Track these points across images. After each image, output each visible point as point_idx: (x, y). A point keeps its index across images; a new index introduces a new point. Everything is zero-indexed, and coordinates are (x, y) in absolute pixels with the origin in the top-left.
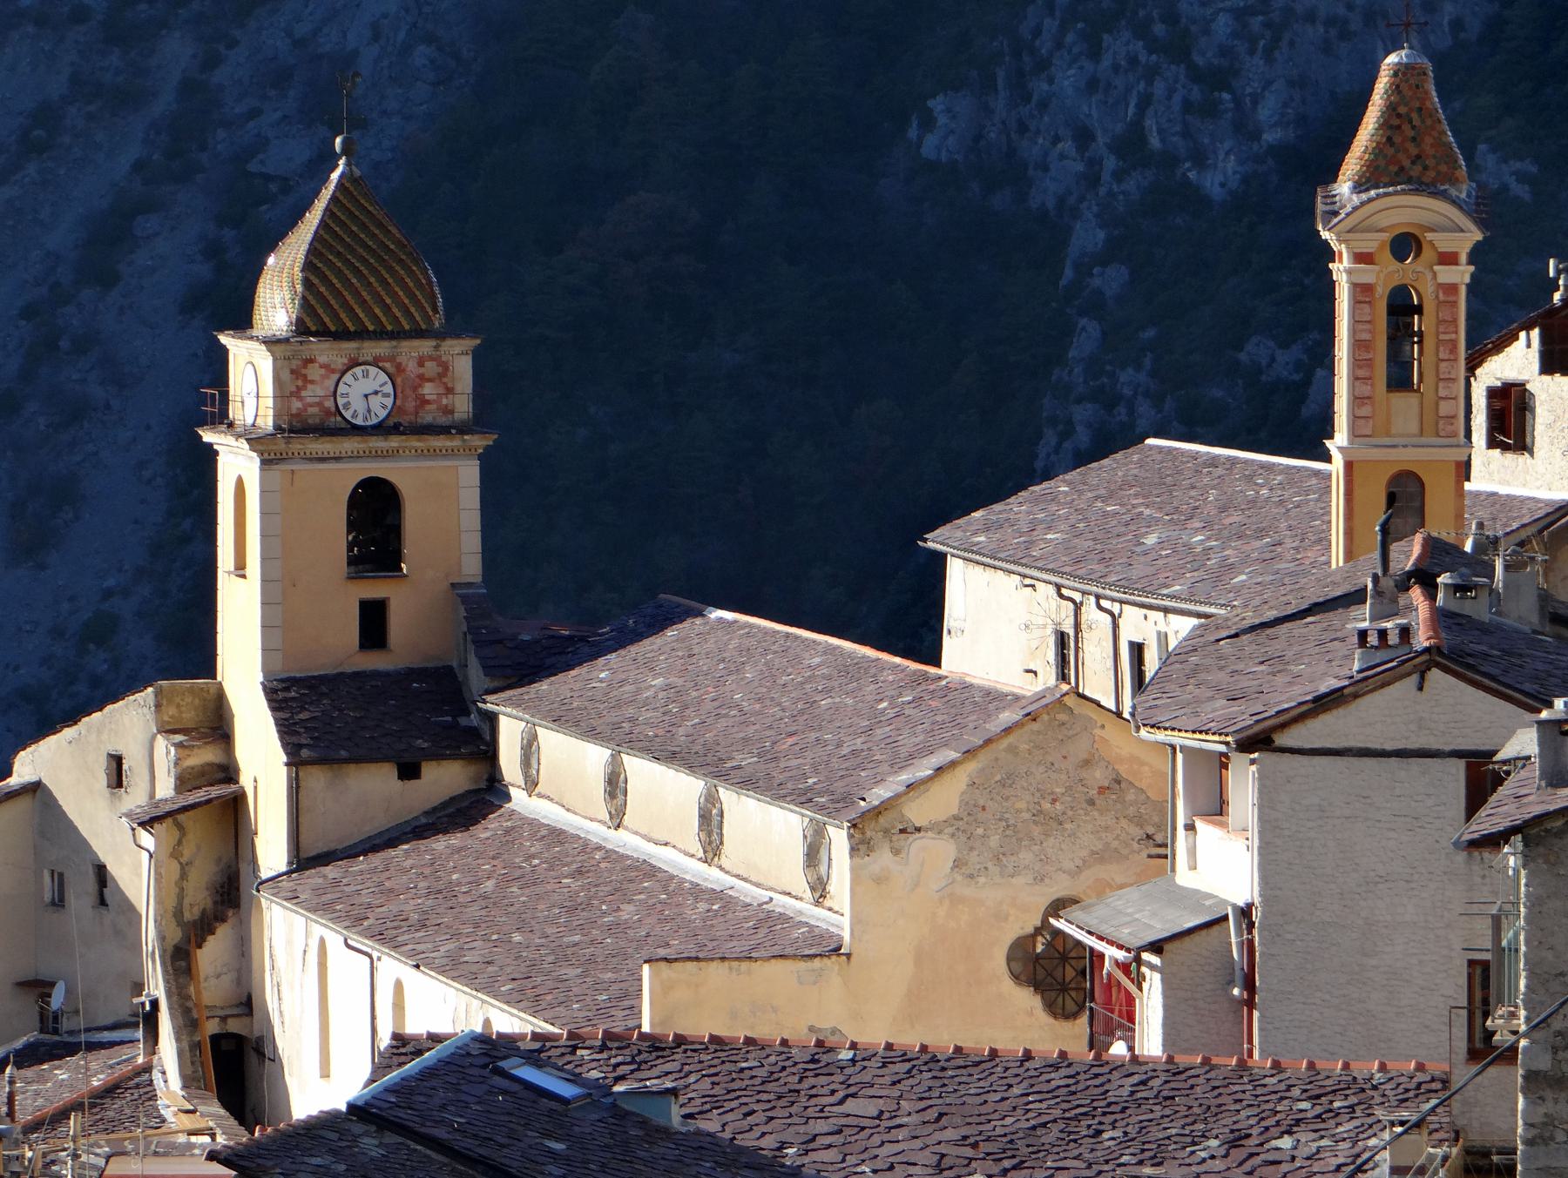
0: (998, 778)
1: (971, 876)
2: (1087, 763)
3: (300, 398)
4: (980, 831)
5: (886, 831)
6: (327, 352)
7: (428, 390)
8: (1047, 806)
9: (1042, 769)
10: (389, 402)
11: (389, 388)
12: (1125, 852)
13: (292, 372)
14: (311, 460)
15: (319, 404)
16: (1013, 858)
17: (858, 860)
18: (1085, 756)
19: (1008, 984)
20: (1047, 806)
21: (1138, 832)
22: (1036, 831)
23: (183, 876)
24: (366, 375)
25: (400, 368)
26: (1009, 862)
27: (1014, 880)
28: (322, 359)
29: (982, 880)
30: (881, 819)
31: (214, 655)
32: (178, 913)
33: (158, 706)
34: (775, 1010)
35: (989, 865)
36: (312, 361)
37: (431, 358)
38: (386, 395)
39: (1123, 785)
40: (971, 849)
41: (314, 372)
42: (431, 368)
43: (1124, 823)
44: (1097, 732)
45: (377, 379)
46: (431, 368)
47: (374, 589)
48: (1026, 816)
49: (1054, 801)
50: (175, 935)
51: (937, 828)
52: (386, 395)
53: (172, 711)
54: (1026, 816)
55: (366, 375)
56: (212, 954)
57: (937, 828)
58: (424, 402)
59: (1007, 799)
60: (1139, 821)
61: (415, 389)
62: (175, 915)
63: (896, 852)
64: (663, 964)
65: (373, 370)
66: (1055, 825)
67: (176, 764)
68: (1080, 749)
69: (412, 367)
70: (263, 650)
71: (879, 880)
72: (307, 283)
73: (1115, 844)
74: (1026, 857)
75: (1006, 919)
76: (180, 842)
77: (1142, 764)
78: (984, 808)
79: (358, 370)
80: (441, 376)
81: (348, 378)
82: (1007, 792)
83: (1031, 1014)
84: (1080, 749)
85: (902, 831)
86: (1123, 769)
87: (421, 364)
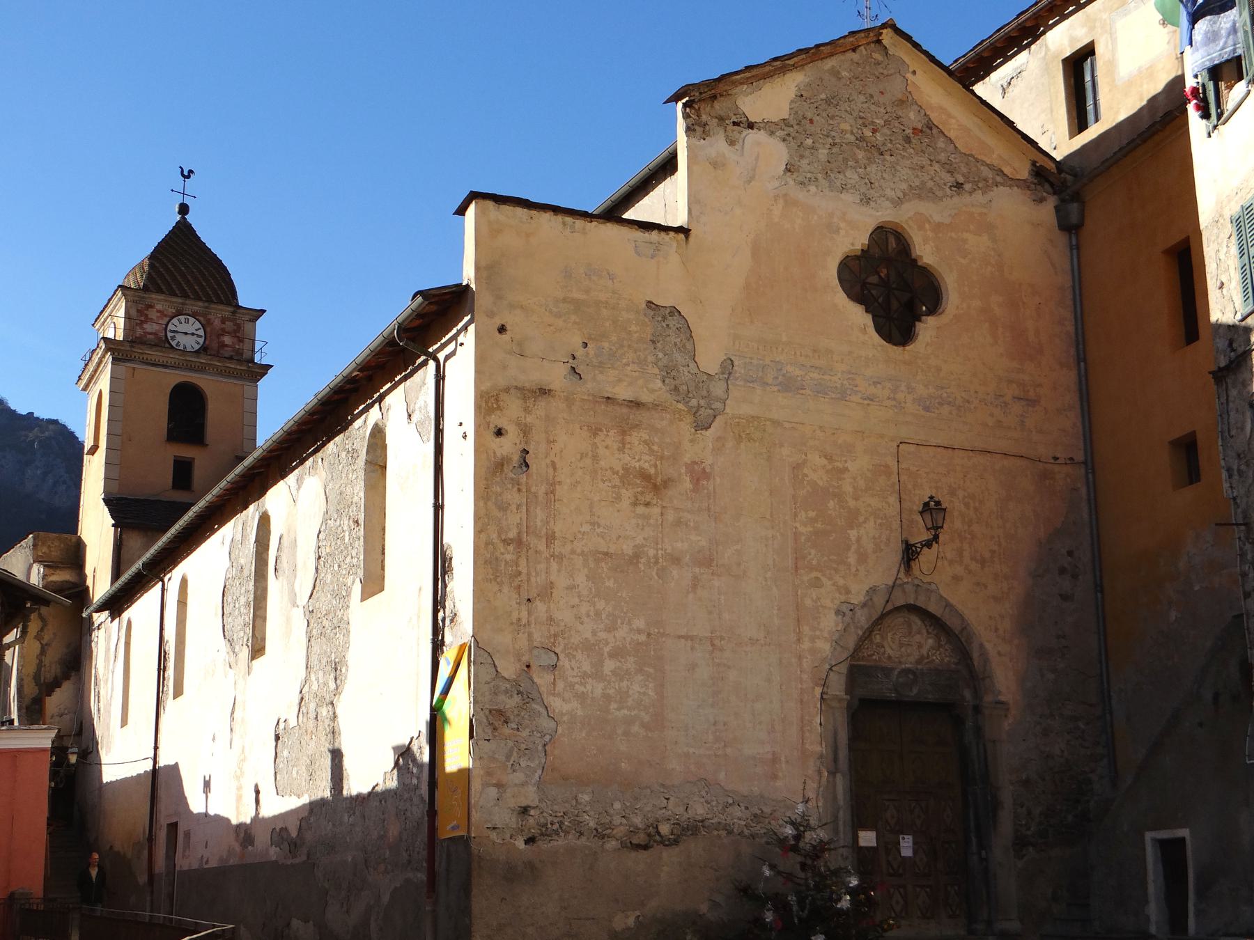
0: (823, 96)
1: (802, 183)
2: (902, 102)
3: (142, 328)
4: (809, 142)
5: (721, 119)
6: (161, 303)
7: (227, 340)
8: (868, 133)
9: (862, 98)
10: (201, 340)
11: (201, 332)
12: (940, 194)
13: (138, 311)
14: (148, 364)
15: (155, 334)
16: (841, 176)
17: (694, 140)
18: (900, 96)
19: (841, 297)
20: (868, 133)
21: (949, 179)
22: (861, 155)
23: (43, 652)
24: (187, 321)
25: (209, 321)
26: (839, 180)
27: (842, 196)
28: (159, 307)
29: (813, 189)
30: (717, 105)
31: (78, 521)
32: (37, 677)
33: (35, 545)
34: (612, 277)
35: (820, 176)
36: (151, 307)
37: (230, 320)
38: (199, 336)
39: (935, 131)
40: (802, 157)
41: (153, 314)
42: (229, 326)
43: (937, 167)
44: (909, 76)
45: (193, 326)
46: (229, 326)
47: (186, 452)
48: (852, 138)
49: (874, 131)
50: (31, 690)
51: (770, 127)
52: (199, 336)
53: (45, 549)
54: (852, 138)
55: (187, 321)
56: (56, 701)
57: (770, 127)
58: (224, 345)
59: (833, 117)
60: (949, 168)
61: (219, 336)
62: (35, 678)
63: (732, 143)
64: (490, 204)
65: (191, 320)
66: (876, 154)
67: (43, 579)
68: (895, 88)
69: (217, 322)
70: (105, 478)
71: (717, 164)
72: (151, 266)
73: (930, 184)
74: (852, 176)
75: (837, 231)
76: (42, 630)
77: (949, 116)
78: (811, 121)
79: (182, 318)
80: (235, 331)
81: (175, 321)
82: (832, 111)
83: (864, 331)
84: (895, 88)
85: (735, 124)
86: (934, 116)
87: (223, 322)
